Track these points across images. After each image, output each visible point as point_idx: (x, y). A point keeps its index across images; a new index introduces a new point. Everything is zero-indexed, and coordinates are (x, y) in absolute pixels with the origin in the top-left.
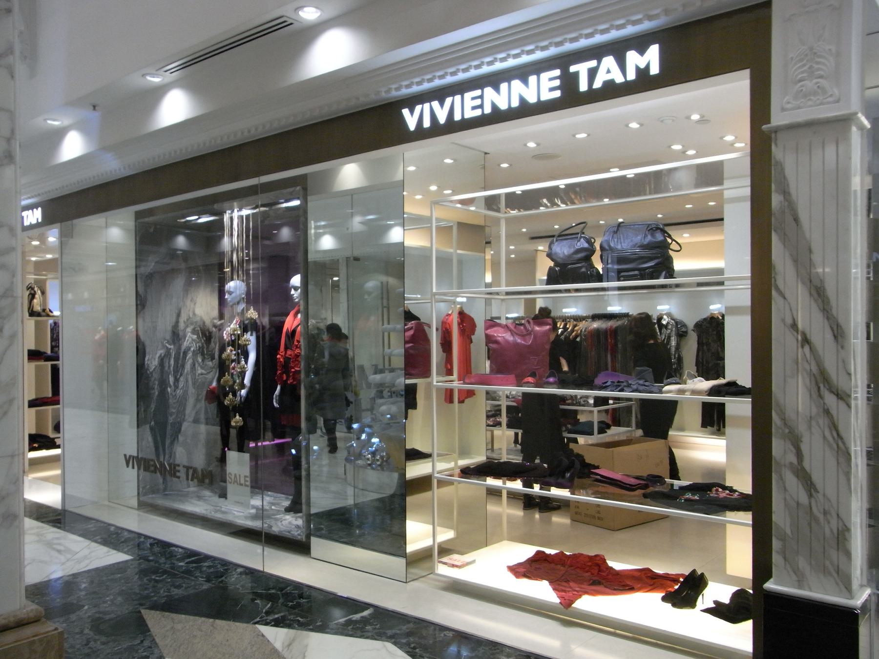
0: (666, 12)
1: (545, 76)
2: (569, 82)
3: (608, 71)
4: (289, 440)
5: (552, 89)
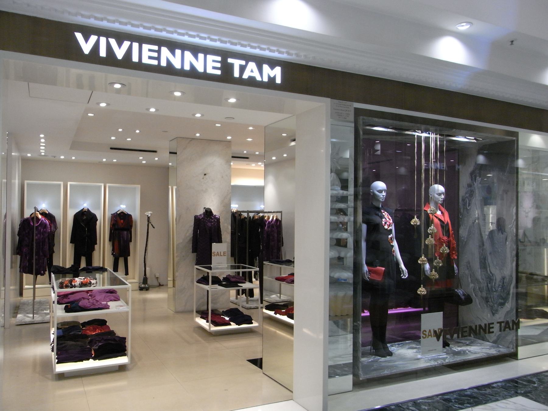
0: (297, 55)
1: (210, 58)
2: (227, 69)
3: (252, 71)
4: (422, 309)
5: (214, 68)
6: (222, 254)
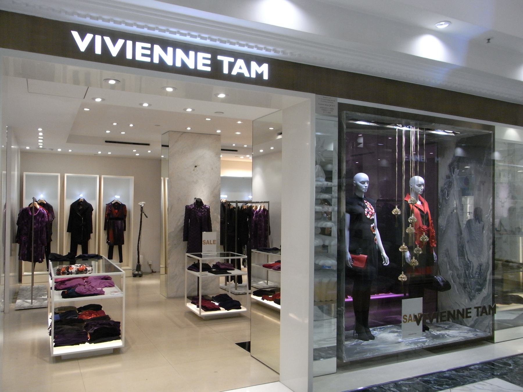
0: (283, 52)
1: (200, 55)
2: (216, 65)
3: (240, 68)
5: (204, 65)
6: (212, 242)
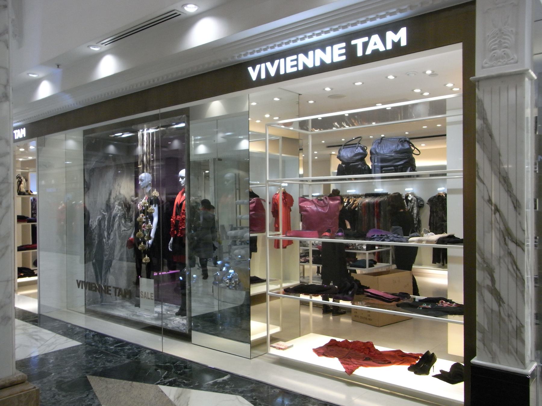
0: (411, 7)
1: (336, 47)
2: (351, 51)
3: (375, 44)
5: (340, 55)
6: (112, 292)
